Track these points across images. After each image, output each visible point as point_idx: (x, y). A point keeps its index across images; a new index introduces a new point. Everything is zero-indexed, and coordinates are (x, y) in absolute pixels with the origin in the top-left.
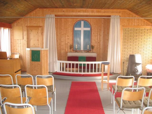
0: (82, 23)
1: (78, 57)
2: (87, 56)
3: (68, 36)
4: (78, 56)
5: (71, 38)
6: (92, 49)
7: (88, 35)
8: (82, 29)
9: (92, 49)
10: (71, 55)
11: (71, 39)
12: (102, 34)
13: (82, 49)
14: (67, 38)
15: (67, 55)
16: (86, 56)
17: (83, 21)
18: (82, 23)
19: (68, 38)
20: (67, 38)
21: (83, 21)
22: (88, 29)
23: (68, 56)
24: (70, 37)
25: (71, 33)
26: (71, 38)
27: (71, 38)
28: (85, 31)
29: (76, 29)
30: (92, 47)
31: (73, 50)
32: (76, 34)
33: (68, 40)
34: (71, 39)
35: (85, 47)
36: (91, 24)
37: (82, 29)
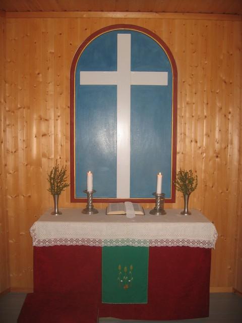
0: (124, 42)
1: (100, 248)
2: (154, 245)
3: (41, 119)
4: (97, 244)
5: (59, 128)
6: (179, 194)
7: (157, 110)
8: (124, 78)
9: (179, 194)
10: (52, 237)
11: (60, 136)
12: (193, 122)
13: (123, 190)
14: (34, 130)
15: (30, 239)
16: (148, 245)
17: (129, 35)
18: (124, 42)
19: (43, 129)
20: (34, 130)
21: (129, 35)
22: (160, 78)
23: (35, 244)
24: (52, 122)
25: (64, 101)
26: (59, 128)
27: (58, 129)
28: (138, 92)
29: (88, 78)
30: (184, 183)
31: (73, 200)
32: (87, 105)
33: (43, 140)
34: (60, 136)
35: (141, 171)
36: (175, 50)
37: (124, 78)
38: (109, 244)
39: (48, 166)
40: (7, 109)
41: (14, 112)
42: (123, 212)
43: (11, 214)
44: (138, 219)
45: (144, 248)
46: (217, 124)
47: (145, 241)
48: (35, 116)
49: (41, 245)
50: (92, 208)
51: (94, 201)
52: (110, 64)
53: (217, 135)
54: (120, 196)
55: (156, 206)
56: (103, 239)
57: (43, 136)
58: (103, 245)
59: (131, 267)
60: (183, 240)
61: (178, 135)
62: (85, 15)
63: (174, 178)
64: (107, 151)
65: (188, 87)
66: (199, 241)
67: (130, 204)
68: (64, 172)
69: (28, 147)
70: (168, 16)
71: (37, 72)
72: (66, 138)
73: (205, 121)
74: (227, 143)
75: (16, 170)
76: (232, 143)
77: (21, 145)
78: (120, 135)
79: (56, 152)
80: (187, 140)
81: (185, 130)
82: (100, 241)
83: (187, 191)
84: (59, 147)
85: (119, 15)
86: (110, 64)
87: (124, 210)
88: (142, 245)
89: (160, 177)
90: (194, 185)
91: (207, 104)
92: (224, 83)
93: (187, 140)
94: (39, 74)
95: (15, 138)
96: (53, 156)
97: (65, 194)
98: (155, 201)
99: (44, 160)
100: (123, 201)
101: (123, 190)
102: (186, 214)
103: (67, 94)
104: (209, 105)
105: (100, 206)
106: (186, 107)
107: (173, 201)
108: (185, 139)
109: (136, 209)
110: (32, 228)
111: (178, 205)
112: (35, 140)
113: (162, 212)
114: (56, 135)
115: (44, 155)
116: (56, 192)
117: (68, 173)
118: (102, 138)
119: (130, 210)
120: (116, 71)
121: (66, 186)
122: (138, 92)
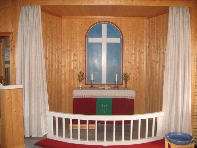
0: (104, 27)
1: (96, 99)
2: (114, 98)
3: (74, 54)
4: (95, 97)
5: (81, 58)
6: (124, 82)
7: (116, 51)
8: (104, 40)
11: (81, 61)
13: (104, 81)
15: (72, 95)
16: (112, 98)
18: (104, 27)
19: (75, 58)
22: (117, 40)
23: (74, 97)
24: (79, 56)
25: (82, 48)
26: (81, 58)
27: (81, 58)
28: (109, 45)
29: (91, 40)
31: (86, 84)
32: (90, 50)
33: (75, 62)
34: (81, 61)
35: (110, 75)
36: (122, 30)
37: (104, 40)
38: (99, 97)
39: (77, 72)
40: (62, 51)
41: (64, 52)
42: (103, 88)
43: (63, 89)
44: (109, 89)
45: (111, 98)
46: (138, 55)
47: (111, 96)
48: (72, 54)
49: (76, 97)
50: (93, 86)
51: (93, 84)
52: (99, 35)
53: (138, 60)
54: (102, 83)
55: (117, 86)
56: (97, 95)
57: (75, 61)
58: (97, 97)
59: (106, 106)
60: (124, 96)
61: (124, 60)
62: (90, 17)
63: (122, 77)
64: (98, 66)
65: (127, 43)
66: (129, 97)
67: (107, 85)
68: (83, 74)
69: (70, 65)
70: (120, 17)
71: (73, 38)
72: (84, 62)
73: (133, 55)
74: (141, 63)
75: (65, 73)
76: (143, 64)
77: (67, 64)
78: (103, 61)
79: (80, 66)
80: (127, 63)
81: (126, 58)
82: (96, 96)
83: (126, 80)
84: (81, 65)
85: (102, 17)
86: (99, 35)
87: (104, 87)
88: (110, 97)
89: (117, 75)
90: (129, 78)
91: (130, 46)
92: (140, 42)
93: (127, 63)
94: (74, 39)
95: (65, 62)
96: (79, 68)
97: (83, 81)
98: (115, 85)
99: (75, 70)
100: (104, 84)
101: (104, 81)
102: (126, 88)
103: (84, 46)
104: (131, 46)
105: (96, 86)
106: (126, 51)
107: (122, 84)
108: (126, 62)
109: (108, 87)
110: (73, 92)
111: (123, 86)
112: (72, 62)
113: (118, 87)
114: (80, 61)
115: (75, 68)
116: (80, 80)
117: (84, 74)
118: (96, 61)
119: (106, 87)
120: (101, 37)
121: (84, 78)
122: (109, 45)
